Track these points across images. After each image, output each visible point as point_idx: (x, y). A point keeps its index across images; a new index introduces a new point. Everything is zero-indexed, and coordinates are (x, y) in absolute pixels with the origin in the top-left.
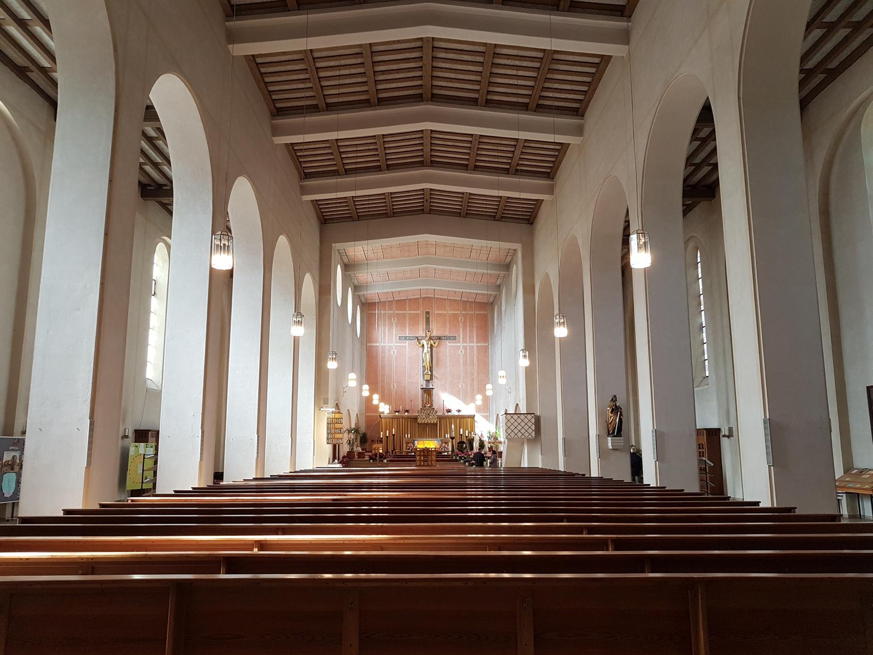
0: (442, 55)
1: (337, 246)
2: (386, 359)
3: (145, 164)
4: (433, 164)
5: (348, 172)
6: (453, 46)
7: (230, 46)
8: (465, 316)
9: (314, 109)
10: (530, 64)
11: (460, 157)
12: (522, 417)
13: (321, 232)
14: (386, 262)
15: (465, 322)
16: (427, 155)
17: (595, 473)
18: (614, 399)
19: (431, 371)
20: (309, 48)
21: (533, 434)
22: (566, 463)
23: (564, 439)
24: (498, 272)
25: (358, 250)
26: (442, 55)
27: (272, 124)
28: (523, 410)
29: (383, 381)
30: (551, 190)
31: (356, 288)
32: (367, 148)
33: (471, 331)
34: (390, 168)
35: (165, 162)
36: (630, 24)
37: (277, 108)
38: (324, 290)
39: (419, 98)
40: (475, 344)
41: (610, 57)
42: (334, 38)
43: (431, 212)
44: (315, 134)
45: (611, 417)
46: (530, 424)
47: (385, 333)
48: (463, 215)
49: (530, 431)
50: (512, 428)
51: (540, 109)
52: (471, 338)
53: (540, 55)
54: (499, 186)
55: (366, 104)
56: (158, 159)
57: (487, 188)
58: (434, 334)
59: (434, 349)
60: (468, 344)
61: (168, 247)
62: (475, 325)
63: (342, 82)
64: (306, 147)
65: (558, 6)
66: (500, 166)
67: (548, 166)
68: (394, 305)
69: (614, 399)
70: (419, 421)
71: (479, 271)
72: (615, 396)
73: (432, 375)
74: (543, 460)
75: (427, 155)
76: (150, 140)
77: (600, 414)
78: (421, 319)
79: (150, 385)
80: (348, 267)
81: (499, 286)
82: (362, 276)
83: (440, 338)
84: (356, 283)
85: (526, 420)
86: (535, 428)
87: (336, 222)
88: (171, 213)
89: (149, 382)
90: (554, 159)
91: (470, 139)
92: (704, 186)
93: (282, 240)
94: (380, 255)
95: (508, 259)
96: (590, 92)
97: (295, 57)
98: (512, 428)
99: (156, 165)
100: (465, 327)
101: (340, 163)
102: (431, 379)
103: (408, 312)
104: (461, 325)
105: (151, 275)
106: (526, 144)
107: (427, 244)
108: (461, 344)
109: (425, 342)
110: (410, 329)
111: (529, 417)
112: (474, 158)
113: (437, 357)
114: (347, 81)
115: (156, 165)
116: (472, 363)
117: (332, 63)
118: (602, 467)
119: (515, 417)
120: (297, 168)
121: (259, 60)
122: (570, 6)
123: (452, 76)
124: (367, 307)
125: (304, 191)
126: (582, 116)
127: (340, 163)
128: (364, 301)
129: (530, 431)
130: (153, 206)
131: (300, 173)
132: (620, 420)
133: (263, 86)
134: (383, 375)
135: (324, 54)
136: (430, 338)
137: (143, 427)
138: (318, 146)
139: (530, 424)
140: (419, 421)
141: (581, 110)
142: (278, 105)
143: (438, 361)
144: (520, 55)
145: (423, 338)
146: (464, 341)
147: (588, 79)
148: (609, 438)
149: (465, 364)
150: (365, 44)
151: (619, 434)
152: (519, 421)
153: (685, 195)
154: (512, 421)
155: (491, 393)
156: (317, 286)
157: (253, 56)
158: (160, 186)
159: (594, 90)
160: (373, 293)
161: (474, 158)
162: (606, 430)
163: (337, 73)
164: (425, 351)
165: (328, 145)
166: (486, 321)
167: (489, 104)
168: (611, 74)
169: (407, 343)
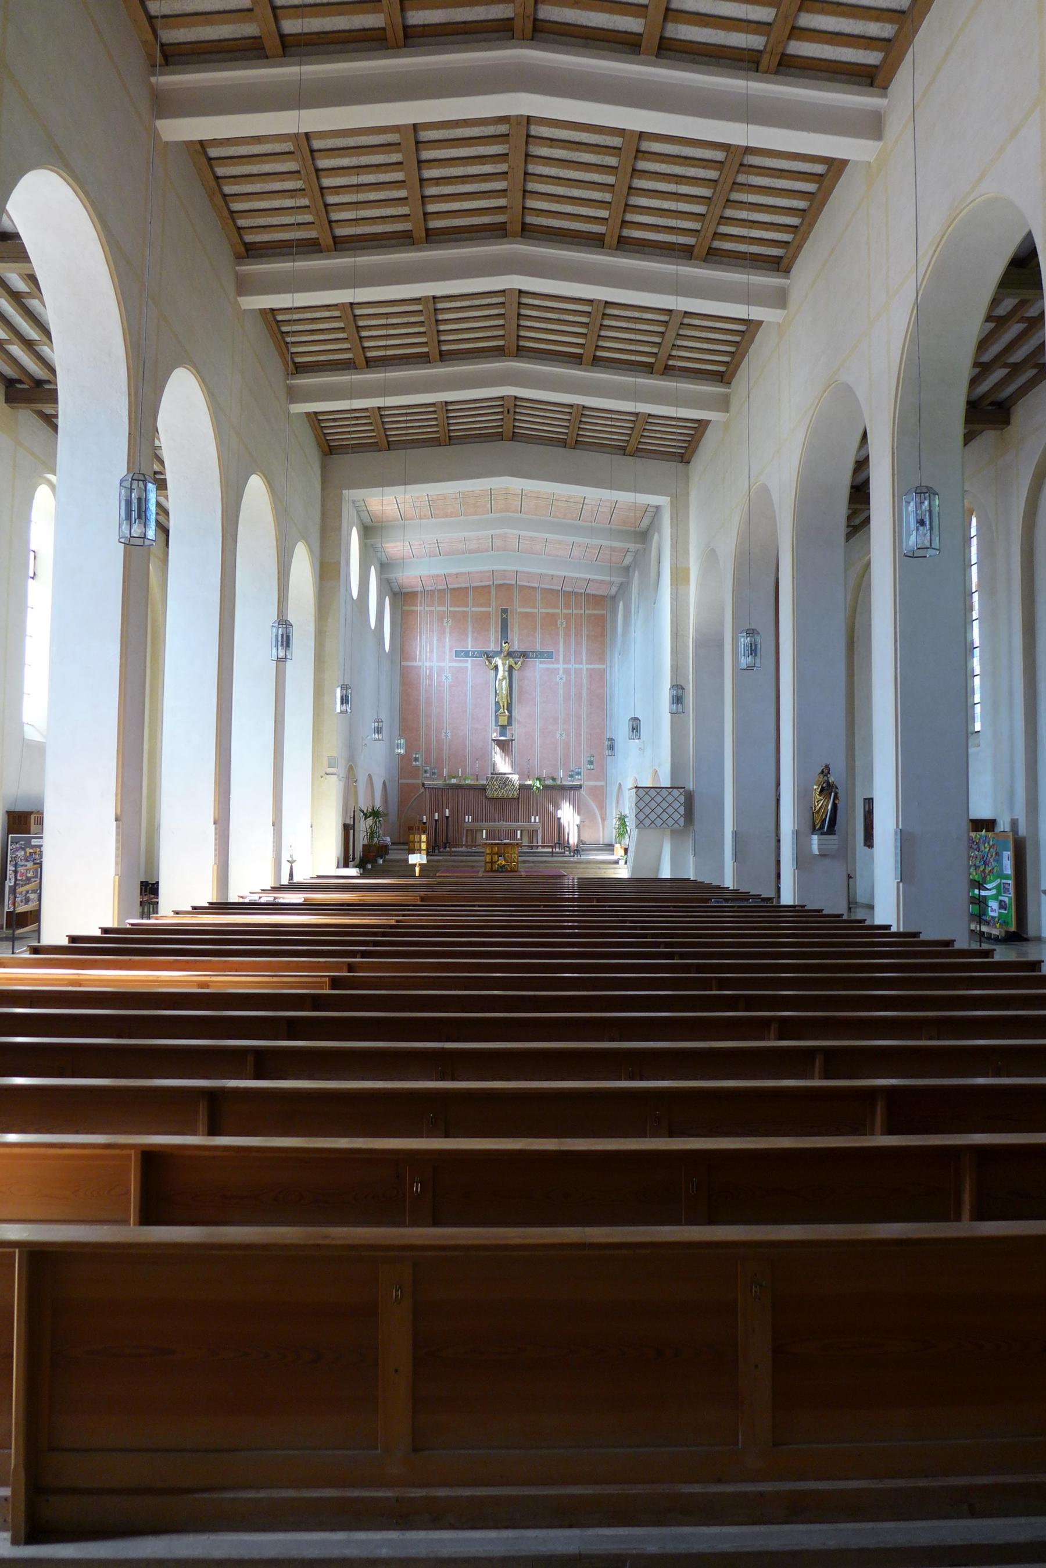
0: (544, 151)
1: (352, 494)
2: (434, 689)
3: (9, 342)
4: (521, 352)
5: (371, 363)
6: (351, 142)
7: (161, 124)
8: (568, 617)
9: (311, 247)
10: (701, 173)
11: (570, 342)
12: (664, 793)
13: (324, 468)
14: (431, 523)
15: (567, 629)
16: (513, 333)
17: (787, 898)
18: (826, 772)
19: (509, 709)
20: (303, 130)
21: (682, 822)
22: (738, 874)
23: (736, 835)
24: (627, 545)
25: (385, 501)
26: (544, 151)
27: (236, 273)
28: (666, 782)
29: (428, 726)
30: (724, 404)
31: (384, 567)
32: (405, 320)
33: (578, 644)
34: (444, 357)
35: (45, 339)
36: (884, 102)
37: (245, 244)
38: (328, 571)
39: (498, 232)
40: (584, 666)
41: (844, 163)
42: (356, 112)
43: (514, 437)
44: (309, 294)
45: (819, 802)
46: (676, 805)
47: (431, 645)
48: (570, 442)
49: (676, 816)
50: (647, 811)
51: (712, 256)
52: (578, 654)
53: (719, 156)
54: (635, 395)
55: (404, 239)
56: (32, 334)
57: (612, 397)
58: (516, 648)
59: (515, 674)
60: (572, 666)
61: (53, 487)
62: (584, 633)
63: (362, 197)
64: (296, 317)
65: (758, 64)
66: (633, 358)
67: (722, 359)
68: (448, 596)
69: (826, 772)
70: (489, 794)
71: (598, 542)
72: (827, 767)
73: (510, 717)
74: (696, 865)
75: (513, 333)
76: (16, 297)
77: (802, 794)
78: (492, 622)
79: (31, 734)
80: (370, 531)
81: (627, 569)
82: (394, 547)
83: (524, 655)
84: (384, 559)
85: (670, 799)
86: (678, 807)
87: (345, 451)
88: (55, 428)
89: (26, 728)
90: (733, 349)
91: (588, 309)
92: (992, 404)
93: (256, 485)
94: (426, 511)
95: (645, 524)
96: (803, 229)
97: (278, 147)
98: (647, 811)
99: (29, 345)
100: (567, 635)
101: (358, 347)
102: (510, 723)
103: (471, 609)
104: (561, 633)
105: (27, 542)
106: (686, 321)
107: (507, 493)
108: (561, 666)
109: (499, 662)
110: (474, 639)
111: (676, 793)
112: (592, 342)
113: (520, 687)
114: (372, 196)
115: (29, 345)
116: (579, 698)
117: (345, 162)
118: (801, 885)
119: (653, 793)
120: (282, 355)
121: (213, 152)
122: (779, 64)
123: (561, 190)
124: (401, 598)
125: (294, 395)
126: (787, 271)
127: (358, 347)
128: (396, 589)
129: (676, 816)
130: (26, 417)
131: (286, 364)
132: (835, 806)
133: (219, 199)
134: (428, 716)
135: (330, 143)
136: (510, 654)
137: (20, 808)
138: (318, 315)
139: (676, 805)
140: (489, 794)
141: (785, 261)
142: (249, 238)
143: (521, 693)
144: (684, 152)
145: (497, 654)
146: (566, 661)
147: (801, 204)
148: (815, 837)
149: (567, 699)
150: (405, 125)
151: (831, 830)
152: (659, 799)
153: (969, 420)
154: (647, 799)
155: (626, 769)
156: (318, 564)
157: (201, 142)
158: (39, 383)
159: (811, 225)
160: (415, 574)
161: (592, 342)
162: (810, 823)
163: (354, 180)
164: (500, 676)
165: (337, 314)
166: (603, 627)
167: (624, 245)
168: (846, 193)
169: (469, 663)
